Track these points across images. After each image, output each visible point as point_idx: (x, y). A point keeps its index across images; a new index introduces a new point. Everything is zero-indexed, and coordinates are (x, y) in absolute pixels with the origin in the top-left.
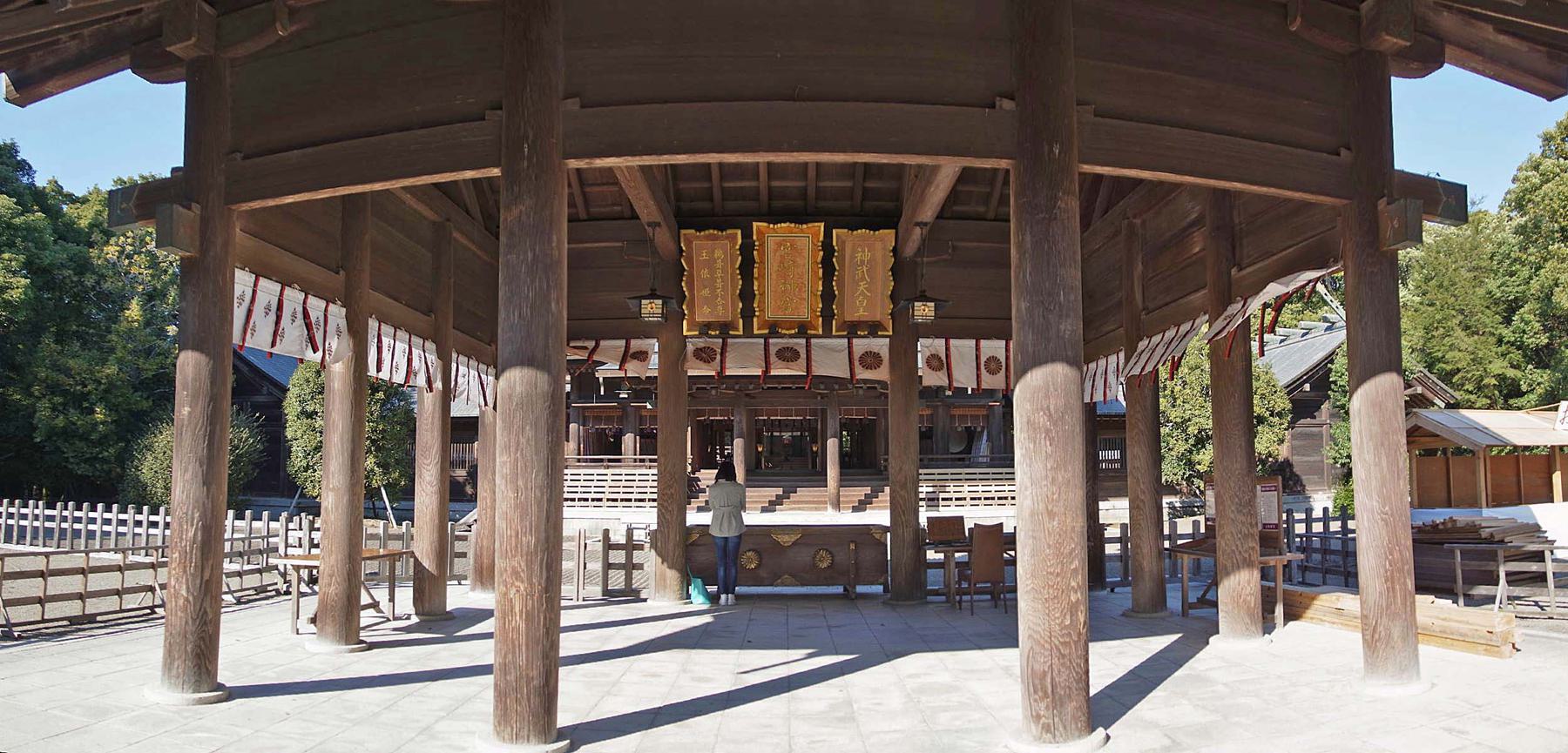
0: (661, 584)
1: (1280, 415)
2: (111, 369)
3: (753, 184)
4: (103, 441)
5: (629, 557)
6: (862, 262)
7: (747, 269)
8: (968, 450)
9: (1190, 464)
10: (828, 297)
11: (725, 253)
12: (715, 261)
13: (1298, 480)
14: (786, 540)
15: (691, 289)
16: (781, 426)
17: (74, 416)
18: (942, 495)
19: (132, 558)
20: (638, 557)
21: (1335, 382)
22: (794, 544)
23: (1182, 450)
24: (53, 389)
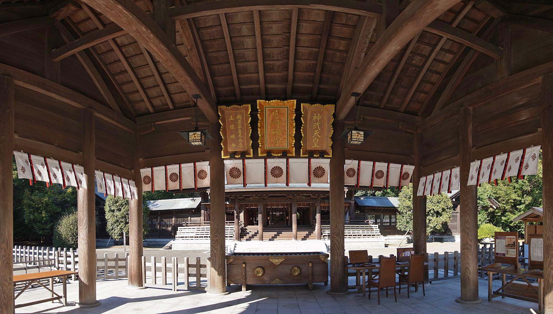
0: (213, 284)
1: (449, 208)
2: (46, 199)
3: (257, 86)
4: (46, 223)
5: (198, 271)
6: (317, 120)
7: (254, 124)
10: (298, 137)
11: (242, 116)
12: (237, 120)
14: (276, 261)
15: (225, 135)
16: (276, 210)
17: (36, 214)
19: (28, 265)
20: (202, 271)
22: (281, 263)
24: (30, 206)
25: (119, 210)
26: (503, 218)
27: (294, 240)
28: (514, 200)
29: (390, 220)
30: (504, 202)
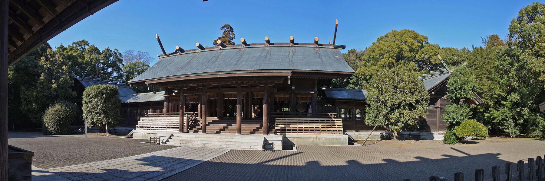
1: (426, 101)
8: (307, 111)
9: (388, 119)
13: (428, 127)
18: (287, 128)
21: (449, 88)
23: (384, 113)
24: (25, 99)
25: (91, 102)
26: (486, 115)
27: (237, 134)
28: (499, 95)
29: (350, 116)
30: (487, 98)
